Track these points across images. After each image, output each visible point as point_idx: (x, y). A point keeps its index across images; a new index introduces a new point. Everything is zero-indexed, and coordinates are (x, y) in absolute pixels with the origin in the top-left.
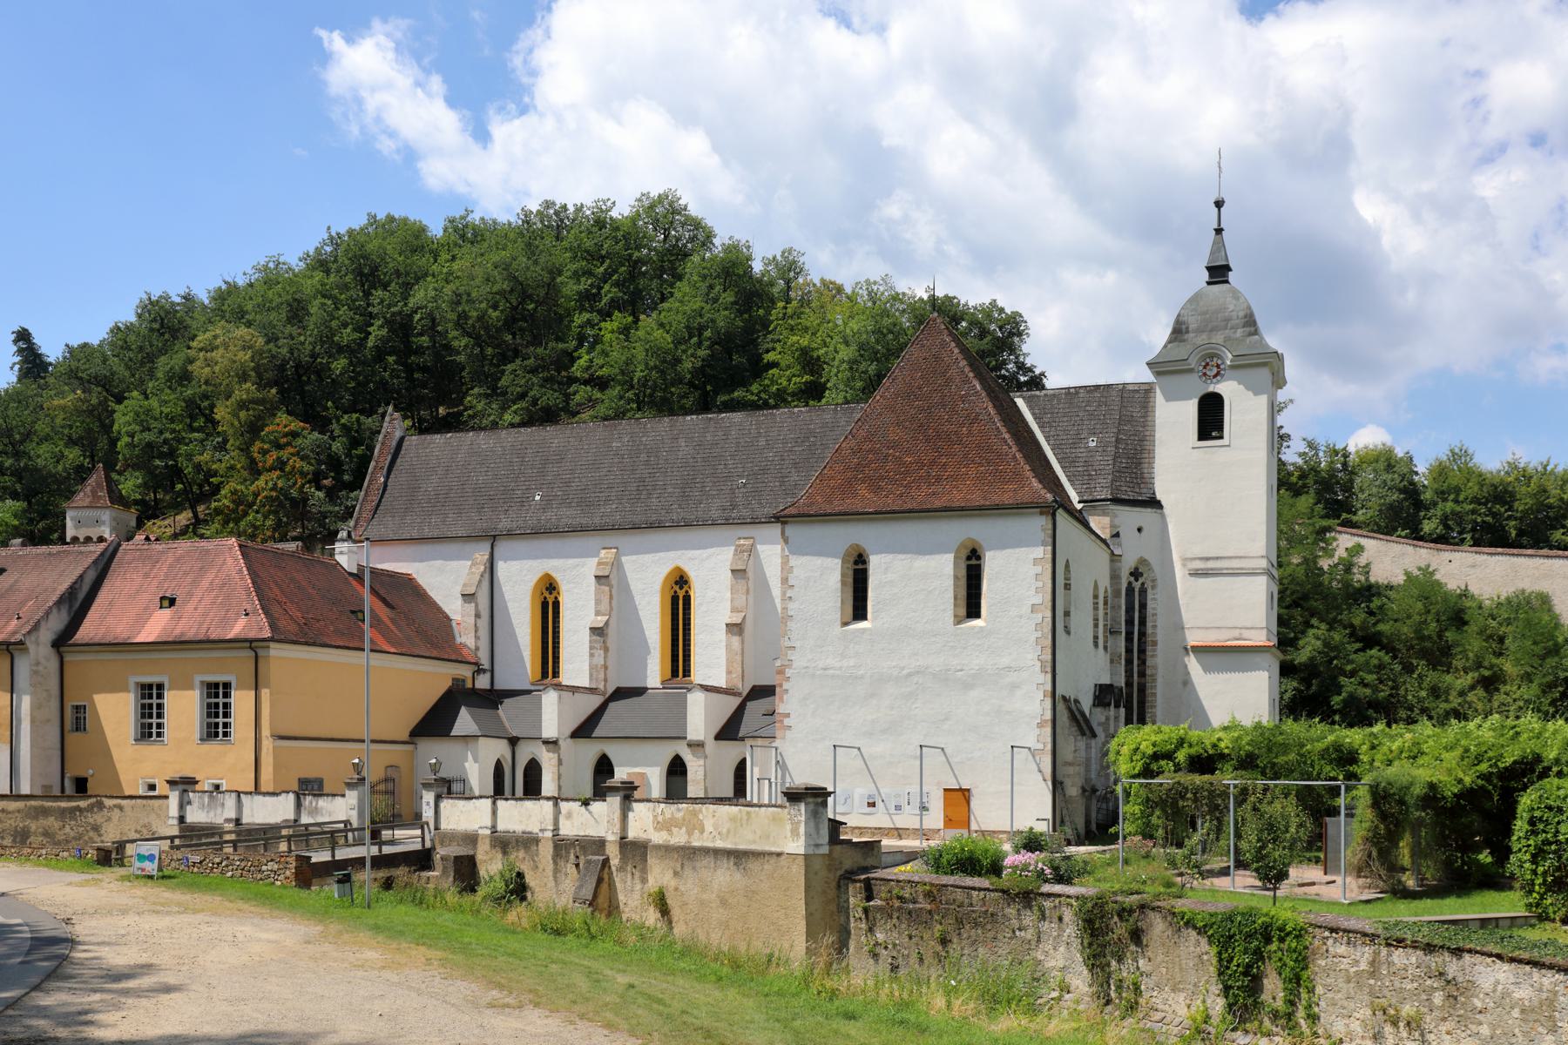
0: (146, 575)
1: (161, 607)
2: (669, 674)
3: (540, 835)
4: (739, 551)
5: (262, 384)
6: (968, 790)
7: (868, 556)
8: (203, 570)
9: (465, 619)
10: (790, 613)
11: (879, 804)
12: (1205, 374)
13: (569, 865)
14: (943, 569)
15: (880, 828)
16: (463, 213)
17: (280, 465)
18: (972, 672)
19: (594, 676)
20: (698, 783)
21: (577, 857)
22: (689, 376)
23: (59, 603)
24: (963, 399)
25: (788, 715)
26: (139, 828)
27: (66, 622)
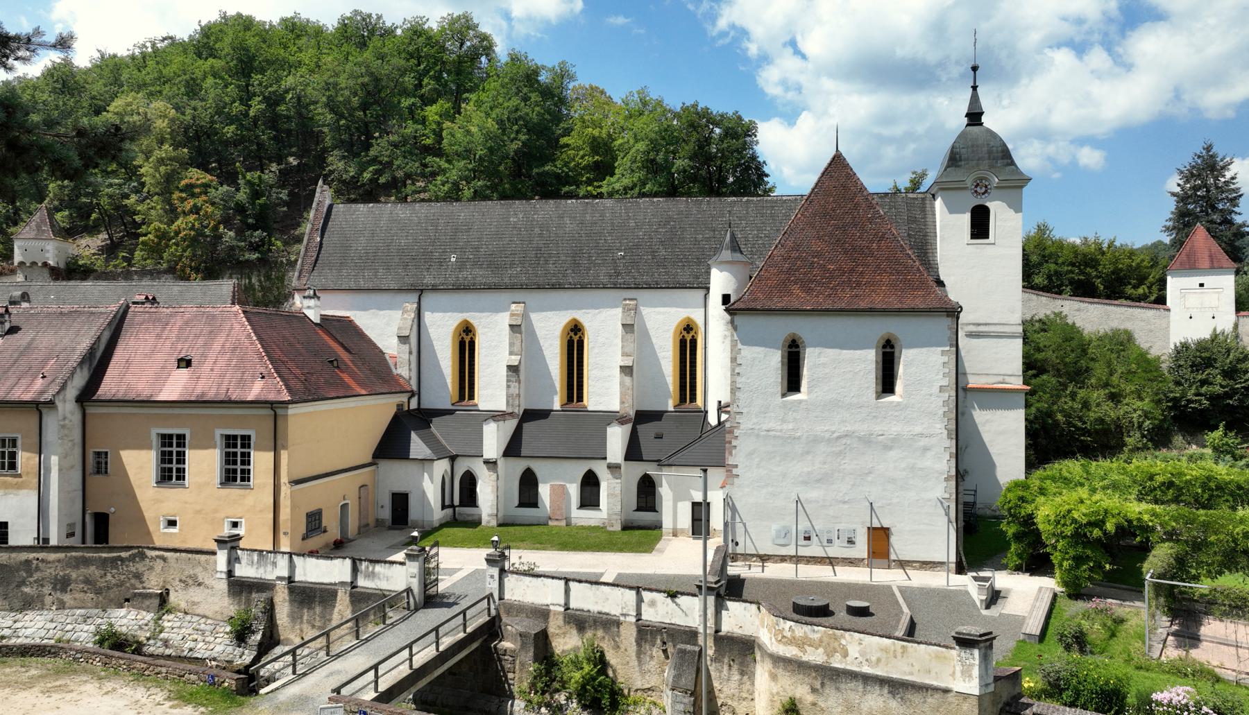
0: (159, 336)
1: (178, 367)
2: (565, 400)
3: (622, 618)
4: (626, 310)
5: (176, 146)
6: (888, 529)
7: (805, 347)
8: (212, 335)
9: (401, 355)
10: (738, 386)
11: (814, 538)
12: (976, 192)
13: (655, 650)
14: (868, 359)
15: (814, 557)
16: (293, 15)
17: (196, 210)
18: (893, 436)
19: (511, 403)
20: (616, 496)
21: (664, 643)
22: (512, 154)
23: (81, 364)
24: (870, 220)
25: (736, 466)
26: (184, 578)
27: (87, 379)
